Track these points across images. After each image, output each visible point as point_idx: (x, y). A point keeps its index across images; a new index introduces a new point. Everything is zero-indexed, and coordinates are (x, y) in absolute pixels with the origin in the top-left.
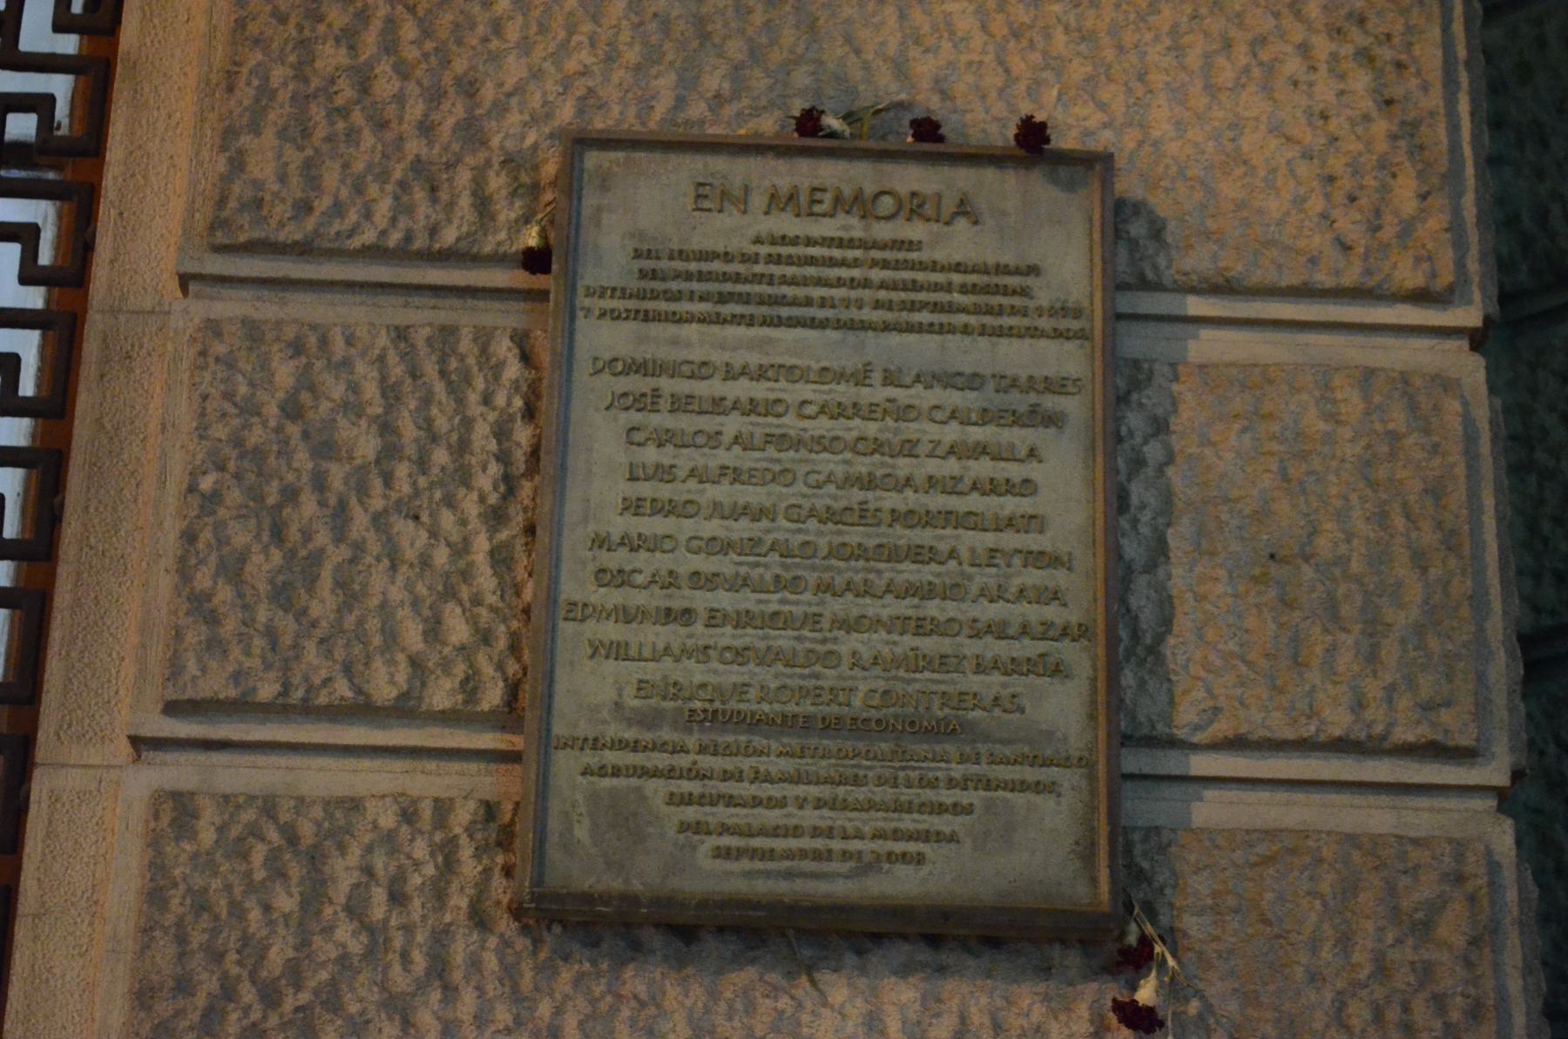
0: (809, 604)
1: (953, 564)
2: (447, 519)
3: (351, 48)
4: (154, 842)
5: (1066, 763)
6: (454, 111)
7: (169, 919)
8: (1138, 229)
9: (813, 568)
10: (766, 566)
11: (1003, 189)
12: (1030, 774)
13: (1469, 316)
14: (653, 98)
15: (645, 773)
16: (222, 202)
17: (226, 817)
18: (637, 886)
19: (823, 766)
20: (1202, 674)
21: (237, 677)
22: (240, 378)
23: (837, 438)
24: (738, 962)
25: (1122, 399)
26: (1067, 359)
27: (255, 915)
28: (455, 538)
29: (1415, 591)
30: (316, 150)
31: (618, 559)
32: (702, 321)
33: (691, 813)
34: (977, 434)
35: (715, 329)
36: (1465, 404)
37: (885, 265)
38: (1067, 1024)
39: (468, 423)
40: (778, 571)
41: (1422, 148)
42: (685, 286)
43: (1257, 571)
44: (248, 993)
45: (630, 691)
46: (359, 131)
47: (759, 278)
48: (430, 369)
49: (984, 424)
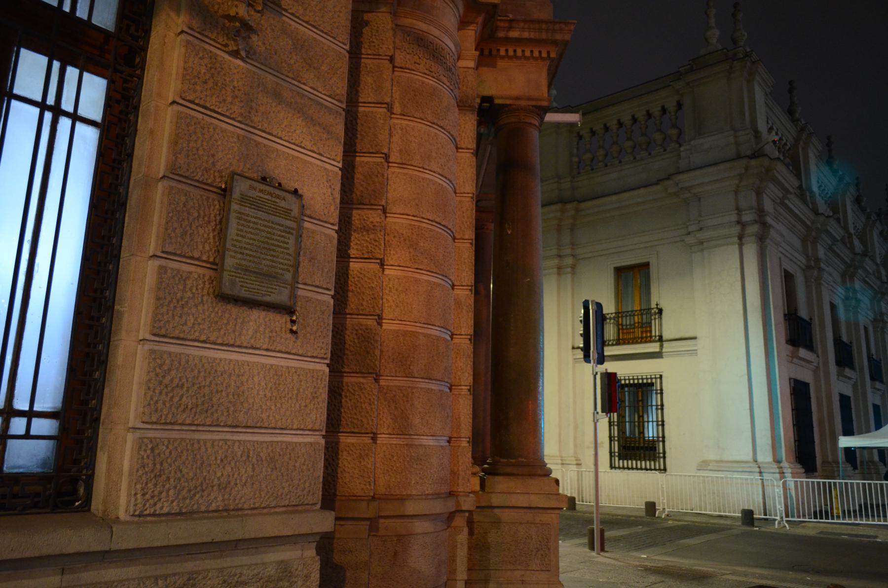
6: (211, 160)
11: (289, 197)
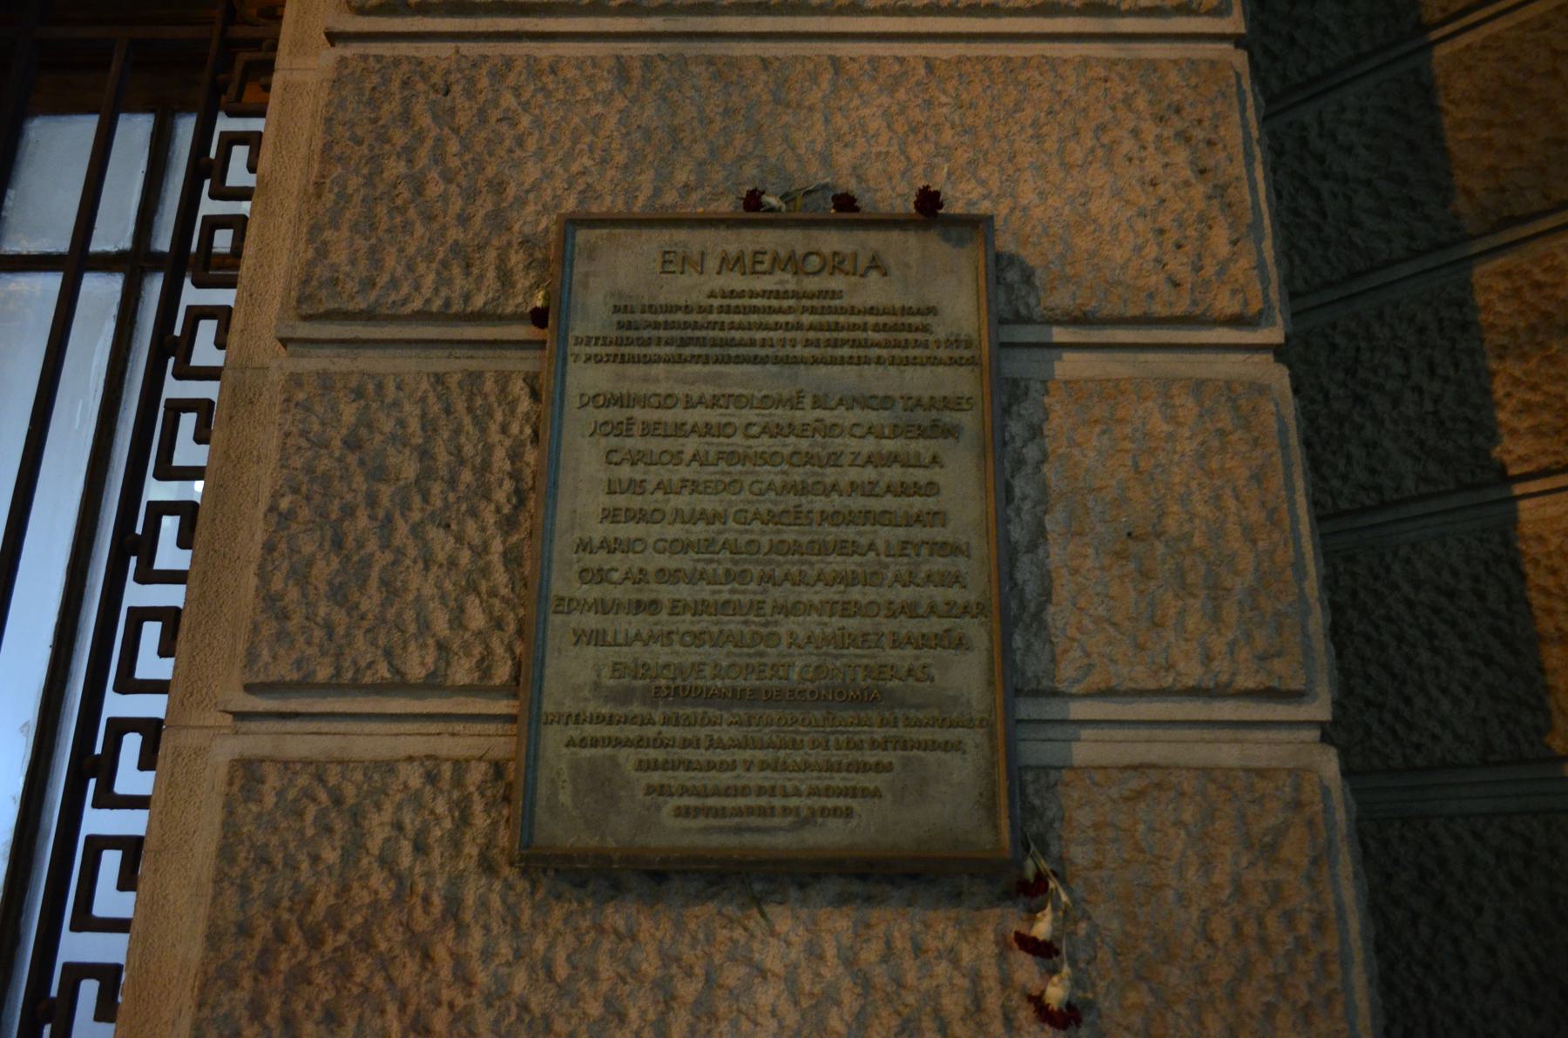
0: (755, 593)
1: (872, 554)
2: (471, 527)
3: (410, 161)
4: (230, 811)
5: (969, 724)
6: (485, 204)
7: (235, 872)
8: (1012, 275)
9: (757, 562)
10: (719, 562)
11: (906, 247)
12: (941, 735)
13: (1274, 334)
14: (637, 189)
15: (618, 743)
16: (306, 282)
17: (286, 781)
18: (611, 843)
19: (767, 733)
20: (1078, 636)
21: (299, 664)
22: (314, 418)
23: (775, 453)
24: (700, 898)
25: (1006, 411)
26: (960, 382)
27: (305, 866)
28: (477, 541)
29: (1247, 561)
30: (379, 240)
31: (599, 559)
32: (667, 361)
33: (656, 777)
34: (889, 445)
35: (677, 367)
36: (1277, 405)
37: (813, 311)
38: (975, 946)
39: (489, 448)
40: (729, 566)
41: (1229, 205)
42: (655, 333)
43: (1118, 547)
44: (296, 937)
45: (606, 672)
46: (413, 223)
47: (712, 325)
48: (461, 406)
49: (896, 437)
